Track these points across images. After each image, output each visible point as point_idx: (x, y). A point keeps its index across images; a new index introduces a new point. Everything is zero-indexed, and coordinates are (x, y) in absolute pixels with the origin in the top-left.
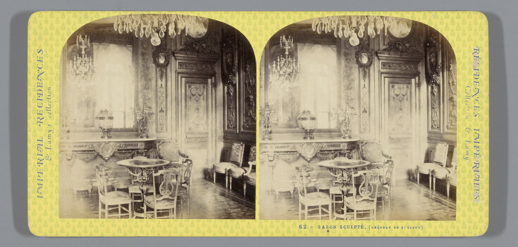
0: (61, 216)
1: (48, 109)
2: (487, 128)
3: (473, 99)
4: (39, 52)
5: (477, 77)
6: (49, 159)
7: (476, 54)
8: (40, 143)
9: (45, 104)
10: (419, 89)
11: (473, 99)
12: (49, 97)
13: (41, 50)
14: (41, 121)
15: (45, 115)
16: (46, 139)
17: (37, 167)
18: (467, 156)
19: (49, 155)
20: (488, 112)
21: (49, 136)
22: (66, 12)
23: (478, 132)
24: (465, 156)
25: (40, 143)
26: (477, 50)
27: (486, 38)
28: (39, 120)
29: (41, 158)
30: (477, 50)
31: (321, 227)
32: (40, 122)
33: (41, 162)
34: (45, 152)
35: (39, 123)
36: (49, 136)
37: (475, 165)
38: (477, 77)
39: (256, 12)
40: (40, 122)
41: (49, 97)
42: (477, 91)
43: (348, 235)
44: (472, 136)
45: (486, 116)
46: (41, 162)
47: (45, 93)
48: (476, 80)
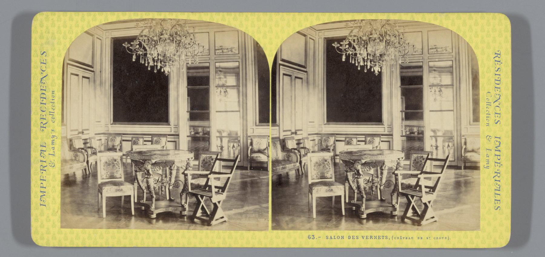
5: (42, 96)
7: (497, 59)
9: (491, 109)
14: (44, 126)
24: (486, 166)
29: (44, 164)
31: (329, 237)
33: (45, 168)
37: (496, 174)
38: (42, 96)
39: (213, 13)
42: (498, 97)
47: (48, 94)
48: (498, 86)
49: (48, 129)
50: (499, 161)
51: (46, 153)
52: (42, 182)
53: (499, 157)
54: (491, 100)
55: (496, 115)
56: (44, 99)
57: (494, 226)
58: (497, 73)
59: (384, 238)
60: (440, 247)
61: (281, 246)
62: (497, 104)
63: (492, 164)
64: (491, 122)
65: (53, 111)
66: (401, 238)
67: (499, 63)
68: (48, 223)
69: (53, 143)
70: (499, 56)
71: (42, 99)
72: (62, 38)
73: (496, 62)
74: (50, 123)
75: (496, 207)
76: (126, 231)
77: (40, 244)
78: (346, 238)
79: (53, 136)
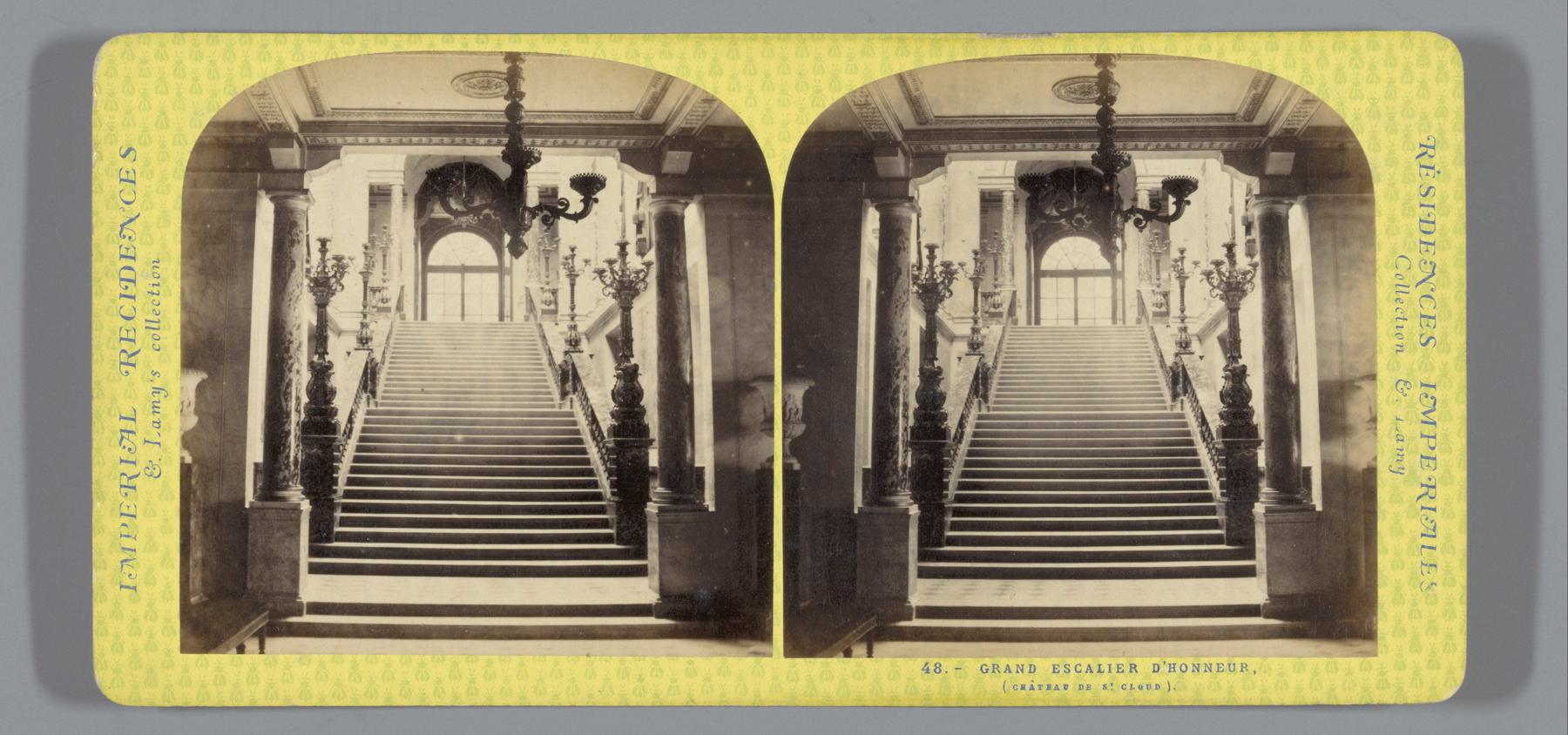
1: (153, 325)
2: (1460, 138)
3: (1416, 293)
6: (156, 473)
7: (1425, 160)
8: (130, 425)
10: (1283, 108)
11: (1416, 293)
12: (155, 289)
16: (144, 421)
17: (121, 499)
19: (156, 462)
20: (1461, 91)
21: (155, 408)
22: (203, 35)
25: (130, 425)
26: (1426, 149)
27: (1457, 105)
28: (124, 357)
29: (130, 470)
30: (1426, 149)
34: (144, 454)
35: (124, 368)
36: (155, 408)
37: (1424, 489)
40: (129, 360)
41: (155, 289)
45: (1456, 338)
46: (131, 483)
51: (137, 440)
52: (125, 519)
53: (124, 531)
58: (1426, 201)
65: (155, 318)
68: (1398, 99)
70: (1431, 152)
71: (124, 284)
72: (156, 102)
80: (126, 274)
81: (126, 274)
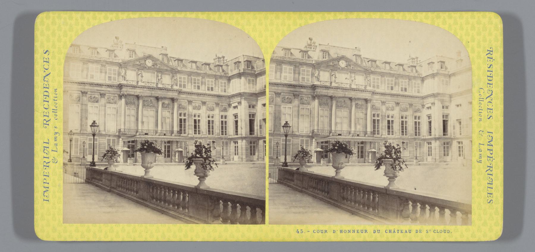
0: (65, 221)
1: (55, 111)
4: (45, 53)
5: (490, 79)
13: (47, 51)
14: (47, 123)
15: (51, 115)
18: (481, 159)
23: (491, 135)
26: (490, 52)
30: (490, 52)
32: (46, 123)
37: (489, 168)
38: (490, 79)
40: (46, 123)
43: (361, 240)
44: (485, 139)
47: (51, 90)
48: (490, 82)
49: (51, 127)
50: (491, 156)
54: (484, 96)
55: (47, 115)
56: (47, 97)
57: (487, 222)
58: (490, 69)
59: (400, 232)
60: (454, 241)
61: (173, 239)
62: (489, 100)
63: (484, 159)
64: (485, 113)
66: (394, 232)
67: (491, 60)
69: (55, 139)
71: (45, 97)
73: (489, 59)
74: (53, 119)
75: (489, 201)
76: (262, 225)
77: (45, 239)
78: (413, 232)
79: (56, 133)
80: (46, 94)
81: (46, 94)
